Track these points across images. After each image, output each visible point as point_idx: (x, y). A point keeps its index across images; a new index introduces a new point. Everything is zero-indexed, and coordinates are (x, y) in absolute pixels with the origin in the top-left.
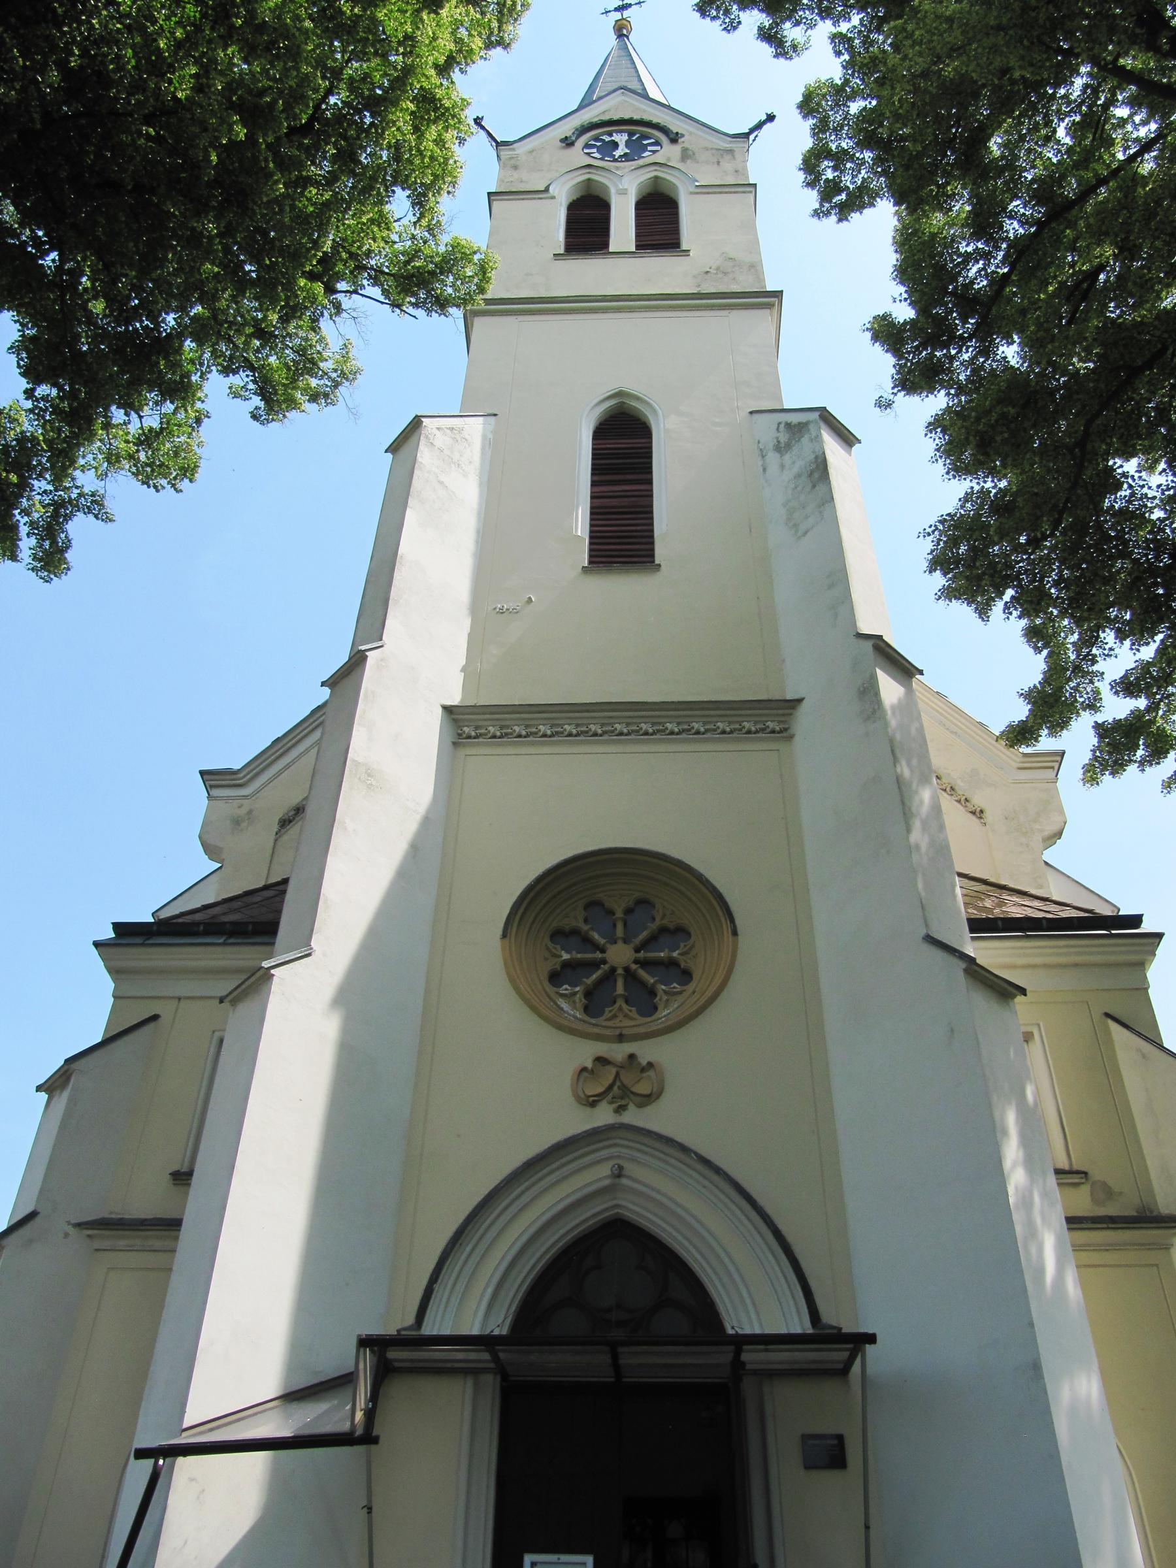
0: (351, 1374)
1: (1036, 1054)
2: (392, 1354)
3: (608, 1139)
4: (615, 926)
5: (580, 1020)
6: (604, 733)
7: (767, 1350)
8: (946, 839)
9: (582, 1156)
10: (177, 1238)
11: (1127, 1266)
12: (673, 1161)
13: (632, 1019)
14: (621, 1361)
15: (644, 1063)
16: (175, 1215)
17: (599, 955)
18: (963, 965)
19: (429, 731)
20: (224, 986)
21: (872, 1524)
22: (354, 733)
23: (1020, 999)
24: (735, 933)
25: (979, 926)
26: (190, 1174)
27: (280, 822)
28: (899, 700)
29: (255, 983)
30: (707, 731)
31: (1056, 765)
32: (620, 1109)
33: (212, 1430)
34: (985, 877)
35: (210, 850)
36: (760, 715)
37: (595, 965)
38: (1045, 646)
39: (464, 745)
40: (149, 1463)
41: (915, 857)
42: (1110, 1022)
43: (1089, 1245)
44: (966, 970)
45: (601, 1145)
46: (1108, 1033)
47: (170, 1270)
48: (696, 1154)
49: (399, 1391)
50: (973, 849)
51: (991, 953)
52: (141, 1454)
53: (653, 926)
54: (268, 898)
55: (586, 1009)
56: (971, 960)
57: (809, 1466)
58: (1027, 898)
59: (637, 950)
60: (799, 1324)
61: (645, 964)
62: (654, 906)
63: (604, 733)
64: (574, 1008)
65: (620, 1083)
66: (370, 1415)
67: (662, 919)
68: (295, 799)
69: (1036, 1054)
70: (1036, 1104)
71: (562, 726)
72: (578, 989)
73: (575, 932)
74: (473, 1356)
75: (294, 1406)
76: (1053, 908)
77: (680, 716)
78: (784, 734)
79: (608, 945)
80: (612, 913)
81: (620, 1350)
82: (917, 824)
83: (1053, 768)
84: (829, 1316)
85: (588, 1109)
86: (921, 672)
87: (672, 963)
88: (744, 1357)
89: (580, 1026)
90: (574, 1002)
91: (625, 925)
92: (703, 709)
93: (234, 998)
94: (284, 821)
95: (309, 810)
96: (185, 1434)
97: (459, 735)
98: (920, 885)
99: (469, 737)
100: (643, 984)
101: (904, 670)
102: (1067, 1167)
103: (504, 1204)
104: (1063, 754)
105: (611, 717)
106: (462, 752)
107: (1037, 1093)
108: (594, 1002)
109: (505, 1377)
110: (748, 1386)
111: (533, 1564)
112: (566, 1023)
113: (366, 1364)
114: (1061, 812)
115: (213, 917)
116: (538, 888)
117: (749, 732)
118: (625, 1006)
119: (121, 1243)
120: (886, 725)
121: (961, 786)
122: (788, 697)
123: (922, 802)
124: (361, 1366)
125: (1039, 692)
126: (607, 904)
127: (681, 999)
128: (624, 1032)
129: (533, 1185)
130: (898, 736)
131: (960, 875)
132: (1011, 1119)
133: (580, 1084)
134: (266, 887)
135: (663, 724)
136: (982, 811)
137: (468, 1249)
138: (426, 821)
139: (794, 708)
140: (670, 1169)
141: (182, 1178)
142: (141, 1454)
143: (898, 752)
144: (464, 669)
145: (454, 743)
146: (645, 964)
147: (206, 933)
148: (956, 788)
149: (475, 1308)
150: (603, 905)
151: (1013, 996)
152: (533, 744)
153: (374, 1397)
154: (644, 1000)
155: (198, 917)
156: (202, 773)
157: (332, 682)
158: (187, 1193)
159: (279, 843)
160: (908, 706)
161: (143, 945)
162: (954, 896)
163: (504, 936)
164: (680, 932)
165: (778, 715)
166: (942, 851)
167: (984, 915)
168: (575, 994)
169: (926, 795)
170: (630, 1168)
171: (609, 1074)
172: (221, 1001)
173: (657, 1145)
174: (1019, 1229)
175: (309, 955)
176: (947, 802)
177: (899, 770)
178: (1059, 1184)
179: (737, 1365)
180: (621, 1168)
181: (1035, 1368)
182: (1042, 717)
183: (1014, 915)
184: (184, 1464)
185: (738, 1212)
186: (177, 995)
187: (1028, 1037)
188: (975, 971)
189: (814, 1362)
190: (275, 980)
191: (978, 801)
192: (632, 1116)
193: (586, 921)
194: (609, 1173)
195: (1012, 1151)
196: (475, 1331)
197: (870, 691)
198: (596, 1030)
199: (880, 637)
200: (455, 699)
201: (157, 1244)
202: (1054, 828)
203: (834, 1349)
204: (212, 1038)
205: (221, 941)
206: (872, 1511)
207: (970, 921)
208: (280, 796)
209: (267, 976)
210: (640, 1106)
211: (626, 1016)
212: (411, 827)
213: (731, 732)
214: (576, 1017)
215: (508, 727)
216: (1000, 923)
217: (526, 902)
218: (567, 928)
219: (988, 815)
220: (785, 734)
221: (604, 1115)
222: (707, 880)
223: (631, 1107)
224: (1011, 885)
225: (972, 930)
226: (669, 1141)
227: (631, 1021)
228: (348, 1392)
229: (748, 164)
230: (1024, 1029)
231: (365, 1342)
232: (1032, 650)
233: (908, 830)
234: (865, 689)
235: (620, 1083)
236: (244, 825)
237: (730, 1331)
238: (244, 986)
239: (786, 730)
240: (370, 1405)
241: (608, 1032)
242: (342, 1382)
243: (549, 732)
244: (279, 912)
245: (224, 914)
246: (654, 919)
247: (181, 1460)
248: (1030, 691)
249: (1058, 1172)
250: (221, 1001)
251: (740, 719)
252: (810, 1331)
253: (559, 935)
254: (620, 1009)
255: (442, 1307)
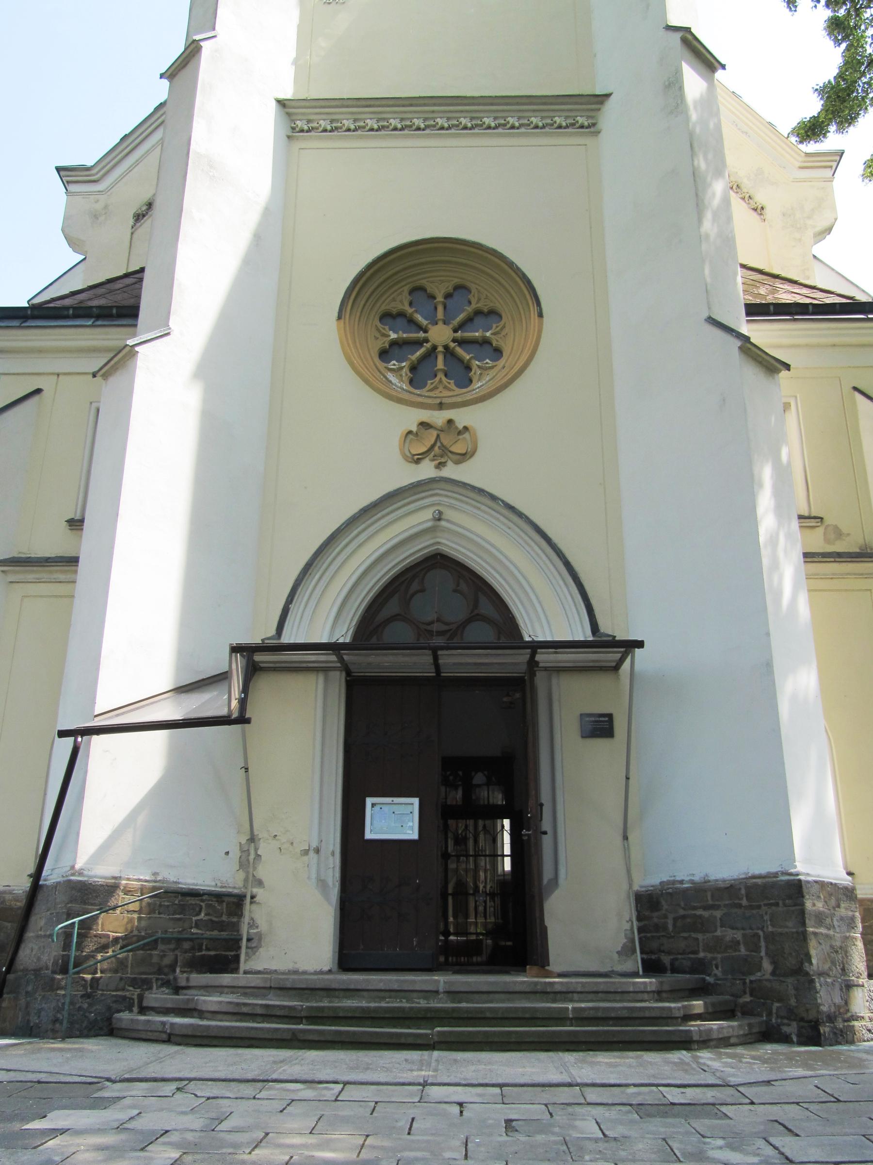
0: (227, 672)
1: (792, 421)
2: (258, 658)
3: (430, 490)
4: (436, 308)
5: (406, 391)
6: (427, 127)
7: (556, 653)
8: (732, 231)
9: (409, 504)
10: (76, 572)
11: (846, 590)
12: (483, 507)
13: (450, 390)
14: (440, 661)
15: (460, 427)
16: (74, 554)
17: (421, 335)
18: (738, 343)
19: (266, 123)
20: (96, 363)
21: (632, 775)
22: (195, 124)
23: (784, 373)
24: (541, 315)
25: (755, 310)
26: (82, 521)
27: (134, 216)
28: (702, 95)
29: (120, 361)
30: (521, 126)
31: (834, 164)
32: (440, 466)
33: (118, 715)
34: (761, 267)
35: (73, 243)
36: (571, 110)
37: (419, 343)
38: (843, 40)
39: (297, 138)
40: (70, 740)
41: (704, 247)
42: (857, 394)
43: (818, 574)
44: (740, 348)
45: (423, 495)
46: (854, 403)
47: (73, 596)
48: (503, 501)
49: (264, 685)
50: (756, 243)
51: (765, 334)
52: (62, 734)
53: (469, 309)
54: (128, 286)
55: (411, 382)
56: (747, 339)
57: (584, 736)
58: (797, 286)
59: (455, 331)
60: (582, 633)
61: (461, 342)
62: (470, 292)
63: (427, 127)
64: (401, 380)
65: (442, 444)
66: (243, 703)
67: (477, 303)
68: (146, 197)
69: (792, 421)
70: (789, 463)
71: (387, 120)
72: (404, 364)
73: (401, 314)
74: (323, 658)
75: (184, 696)
76: (819, 295)
77: (497, 111)
78: (591, 128)
79: (430, 326)
80: (433, 297)
81: (440, 652)
82: (708, 216)
83: (831, 167)
84: (606, 627)
85: (414, 466)
86: (723, 67)
87: (486, 342)
88: (538, 658)
89: (406, 396)
90: (401, 375)
91: (445, 308)
92: (518, 104)
93: (105, 372)
94: (138, 215)
95: (157, 205)
96: (96, 719)
97: (293, 128)
98: (707, 272)
99: (302, 131)
100: (460, 360)
101: (708, 63)
102: (806, 514)
103: (344, 543)
104: (841, 154)
105: (433, 112)
106: (297, 145)
107: (790, 455)
108: (418, 375)
109: (348, 673)
110: (540, 678)
111: (373, 805)
112: (394, 393)
113: (238, 665)
114: (833, 208)
115: (81, 302)
116: (368, 274)
117: (560, 127)
118: (444, 378)
119: (30, 577)
120: (687, 119)
121: (747, 185)
122: (597, 93)
123: (714, 194)
124: (234, 666)
125: (833, 88)
126: (429, 290)
127: (492, 373)
128: (444, 401)
129: (369, 526)
130: (698, 130)
131: (743, 266)
132: (767, 474)
133: (407, 445)
134: (126, 275)
135: (481, 119)
136: (762, 208)
137: (317, 577)
138: (267, 212)
139: (602, 103)
140: (482, 514)
141: (76, 524)
142: (62, 734)
143: (695, 145)
144: (295, 62)
145: (289, 137)
146: (461, 342)
147: (76, 316)
148: (742, 186)
149: (325, 620)
150: (425, 290)
151: (778, 371)
152: (361, 137)
153: (245, 689)
154: (462, 374)
155: (67, 302)
156: (59, 169)
157: (171, 74)
158: (81, 537)
159: (135, 236)
160: (709, 102)
161: (20, 327)
162: (735, 284)
163: (339, 317)
164: (493, 313)
165: (588, 110)
166: (728, 242)
167: (758, 301)
168: (402, 368)
169: (718, 187)
170: (449, 514)
171: (432, 435)
172: (94, 375)
173: (472, 495)
174: (766, 561)
175: (168, 334)
176: (735, 200)
177: (696, 163)
178: (801, 527)
179: (533, 664)
180: (440, 513)
181: (769, 666)
182: (833, 112)
183: (784, 301)
184: (97, 740)
185: (536, 548)
186: (57, 371)
187: (786, 407)
188: (749, 349)
189: (593, 661)
190: (140, 357)
191: (760, 198)
192: (451, 471)
193: (411, 304)
194: (431, 517)
195: (765, 501)
196: (324, 640)
197: (674, 85)
198: (420, 399)
199: (688, 30)
200: (287, 93)
201: (62, 577)
202: (826, 224)
203: (609, 652)
204: (90, 408)
205: (90, 323)
206: (632, 767)
207: (747, 305)
208: (133, 180)
209: (132, 353)
210: (457, 462)
211: (445, 387)
212: (252, 218)
213: (543, 127)
214: (403, 389)
215: (337, 121)
216: (772, 308)
217: (357, 289)
218: (394, 311)
219: (768, 212)
220: (592, 129)
221: (427, 470)
222: (518, 268)
223: (450, 463)
224: (783, 275)
225: (748, 314)
226: (481, 491)
227: (450, 391)
228: (224, 686)
229: (294, 55)
230: (785, 400)
231: (236, 649)
232: (832, 43)
233: (700, 221)
234: (669, 84)
235: (442, 444)
236: (102, 218)
237: (527, 639)
238: (112, 362)
239: (594, 125)
240: (243, 695)
241: (429, 401)
242: (222, 678)
243: (376, 127)
244: (138, 297)
245: (90, 299)
246: (470, 303)
247: (95, 738)
248: (825, 87)
249: (801, 517)
250: (94, 375)
251: (551, 114)
252: (591, 639)
253: (387, 317)
254: (441, 381)
255: (296, 624)
